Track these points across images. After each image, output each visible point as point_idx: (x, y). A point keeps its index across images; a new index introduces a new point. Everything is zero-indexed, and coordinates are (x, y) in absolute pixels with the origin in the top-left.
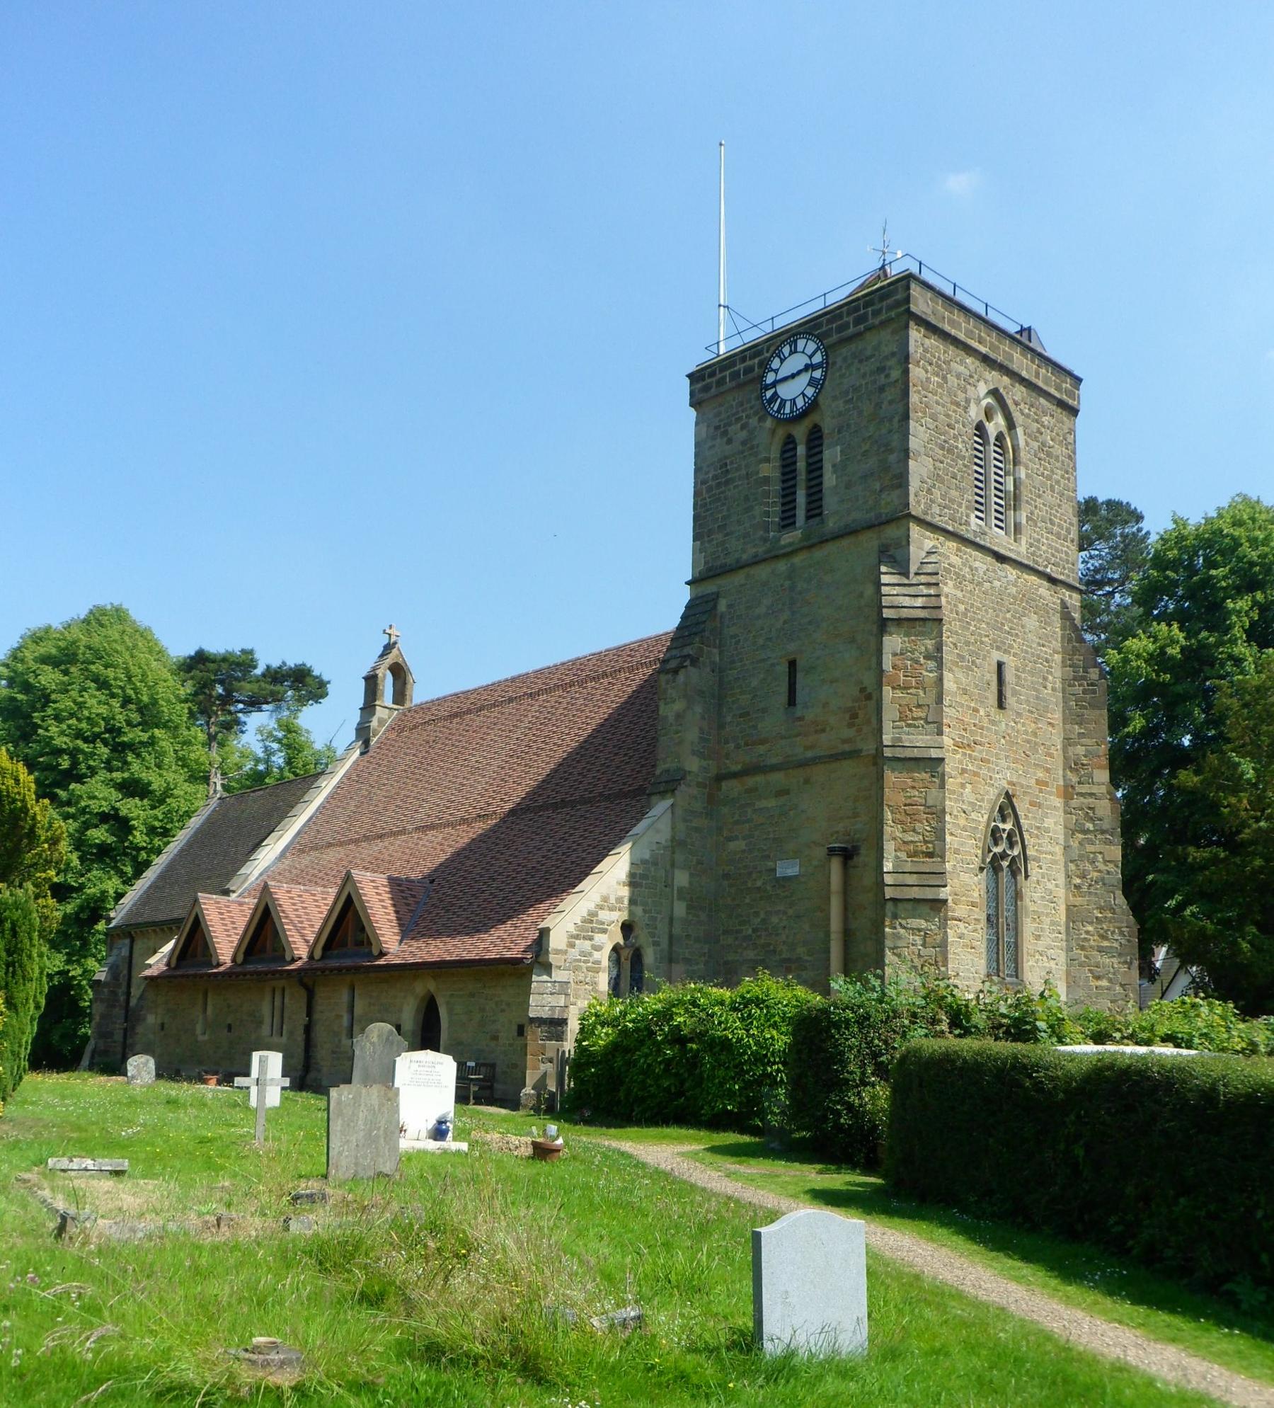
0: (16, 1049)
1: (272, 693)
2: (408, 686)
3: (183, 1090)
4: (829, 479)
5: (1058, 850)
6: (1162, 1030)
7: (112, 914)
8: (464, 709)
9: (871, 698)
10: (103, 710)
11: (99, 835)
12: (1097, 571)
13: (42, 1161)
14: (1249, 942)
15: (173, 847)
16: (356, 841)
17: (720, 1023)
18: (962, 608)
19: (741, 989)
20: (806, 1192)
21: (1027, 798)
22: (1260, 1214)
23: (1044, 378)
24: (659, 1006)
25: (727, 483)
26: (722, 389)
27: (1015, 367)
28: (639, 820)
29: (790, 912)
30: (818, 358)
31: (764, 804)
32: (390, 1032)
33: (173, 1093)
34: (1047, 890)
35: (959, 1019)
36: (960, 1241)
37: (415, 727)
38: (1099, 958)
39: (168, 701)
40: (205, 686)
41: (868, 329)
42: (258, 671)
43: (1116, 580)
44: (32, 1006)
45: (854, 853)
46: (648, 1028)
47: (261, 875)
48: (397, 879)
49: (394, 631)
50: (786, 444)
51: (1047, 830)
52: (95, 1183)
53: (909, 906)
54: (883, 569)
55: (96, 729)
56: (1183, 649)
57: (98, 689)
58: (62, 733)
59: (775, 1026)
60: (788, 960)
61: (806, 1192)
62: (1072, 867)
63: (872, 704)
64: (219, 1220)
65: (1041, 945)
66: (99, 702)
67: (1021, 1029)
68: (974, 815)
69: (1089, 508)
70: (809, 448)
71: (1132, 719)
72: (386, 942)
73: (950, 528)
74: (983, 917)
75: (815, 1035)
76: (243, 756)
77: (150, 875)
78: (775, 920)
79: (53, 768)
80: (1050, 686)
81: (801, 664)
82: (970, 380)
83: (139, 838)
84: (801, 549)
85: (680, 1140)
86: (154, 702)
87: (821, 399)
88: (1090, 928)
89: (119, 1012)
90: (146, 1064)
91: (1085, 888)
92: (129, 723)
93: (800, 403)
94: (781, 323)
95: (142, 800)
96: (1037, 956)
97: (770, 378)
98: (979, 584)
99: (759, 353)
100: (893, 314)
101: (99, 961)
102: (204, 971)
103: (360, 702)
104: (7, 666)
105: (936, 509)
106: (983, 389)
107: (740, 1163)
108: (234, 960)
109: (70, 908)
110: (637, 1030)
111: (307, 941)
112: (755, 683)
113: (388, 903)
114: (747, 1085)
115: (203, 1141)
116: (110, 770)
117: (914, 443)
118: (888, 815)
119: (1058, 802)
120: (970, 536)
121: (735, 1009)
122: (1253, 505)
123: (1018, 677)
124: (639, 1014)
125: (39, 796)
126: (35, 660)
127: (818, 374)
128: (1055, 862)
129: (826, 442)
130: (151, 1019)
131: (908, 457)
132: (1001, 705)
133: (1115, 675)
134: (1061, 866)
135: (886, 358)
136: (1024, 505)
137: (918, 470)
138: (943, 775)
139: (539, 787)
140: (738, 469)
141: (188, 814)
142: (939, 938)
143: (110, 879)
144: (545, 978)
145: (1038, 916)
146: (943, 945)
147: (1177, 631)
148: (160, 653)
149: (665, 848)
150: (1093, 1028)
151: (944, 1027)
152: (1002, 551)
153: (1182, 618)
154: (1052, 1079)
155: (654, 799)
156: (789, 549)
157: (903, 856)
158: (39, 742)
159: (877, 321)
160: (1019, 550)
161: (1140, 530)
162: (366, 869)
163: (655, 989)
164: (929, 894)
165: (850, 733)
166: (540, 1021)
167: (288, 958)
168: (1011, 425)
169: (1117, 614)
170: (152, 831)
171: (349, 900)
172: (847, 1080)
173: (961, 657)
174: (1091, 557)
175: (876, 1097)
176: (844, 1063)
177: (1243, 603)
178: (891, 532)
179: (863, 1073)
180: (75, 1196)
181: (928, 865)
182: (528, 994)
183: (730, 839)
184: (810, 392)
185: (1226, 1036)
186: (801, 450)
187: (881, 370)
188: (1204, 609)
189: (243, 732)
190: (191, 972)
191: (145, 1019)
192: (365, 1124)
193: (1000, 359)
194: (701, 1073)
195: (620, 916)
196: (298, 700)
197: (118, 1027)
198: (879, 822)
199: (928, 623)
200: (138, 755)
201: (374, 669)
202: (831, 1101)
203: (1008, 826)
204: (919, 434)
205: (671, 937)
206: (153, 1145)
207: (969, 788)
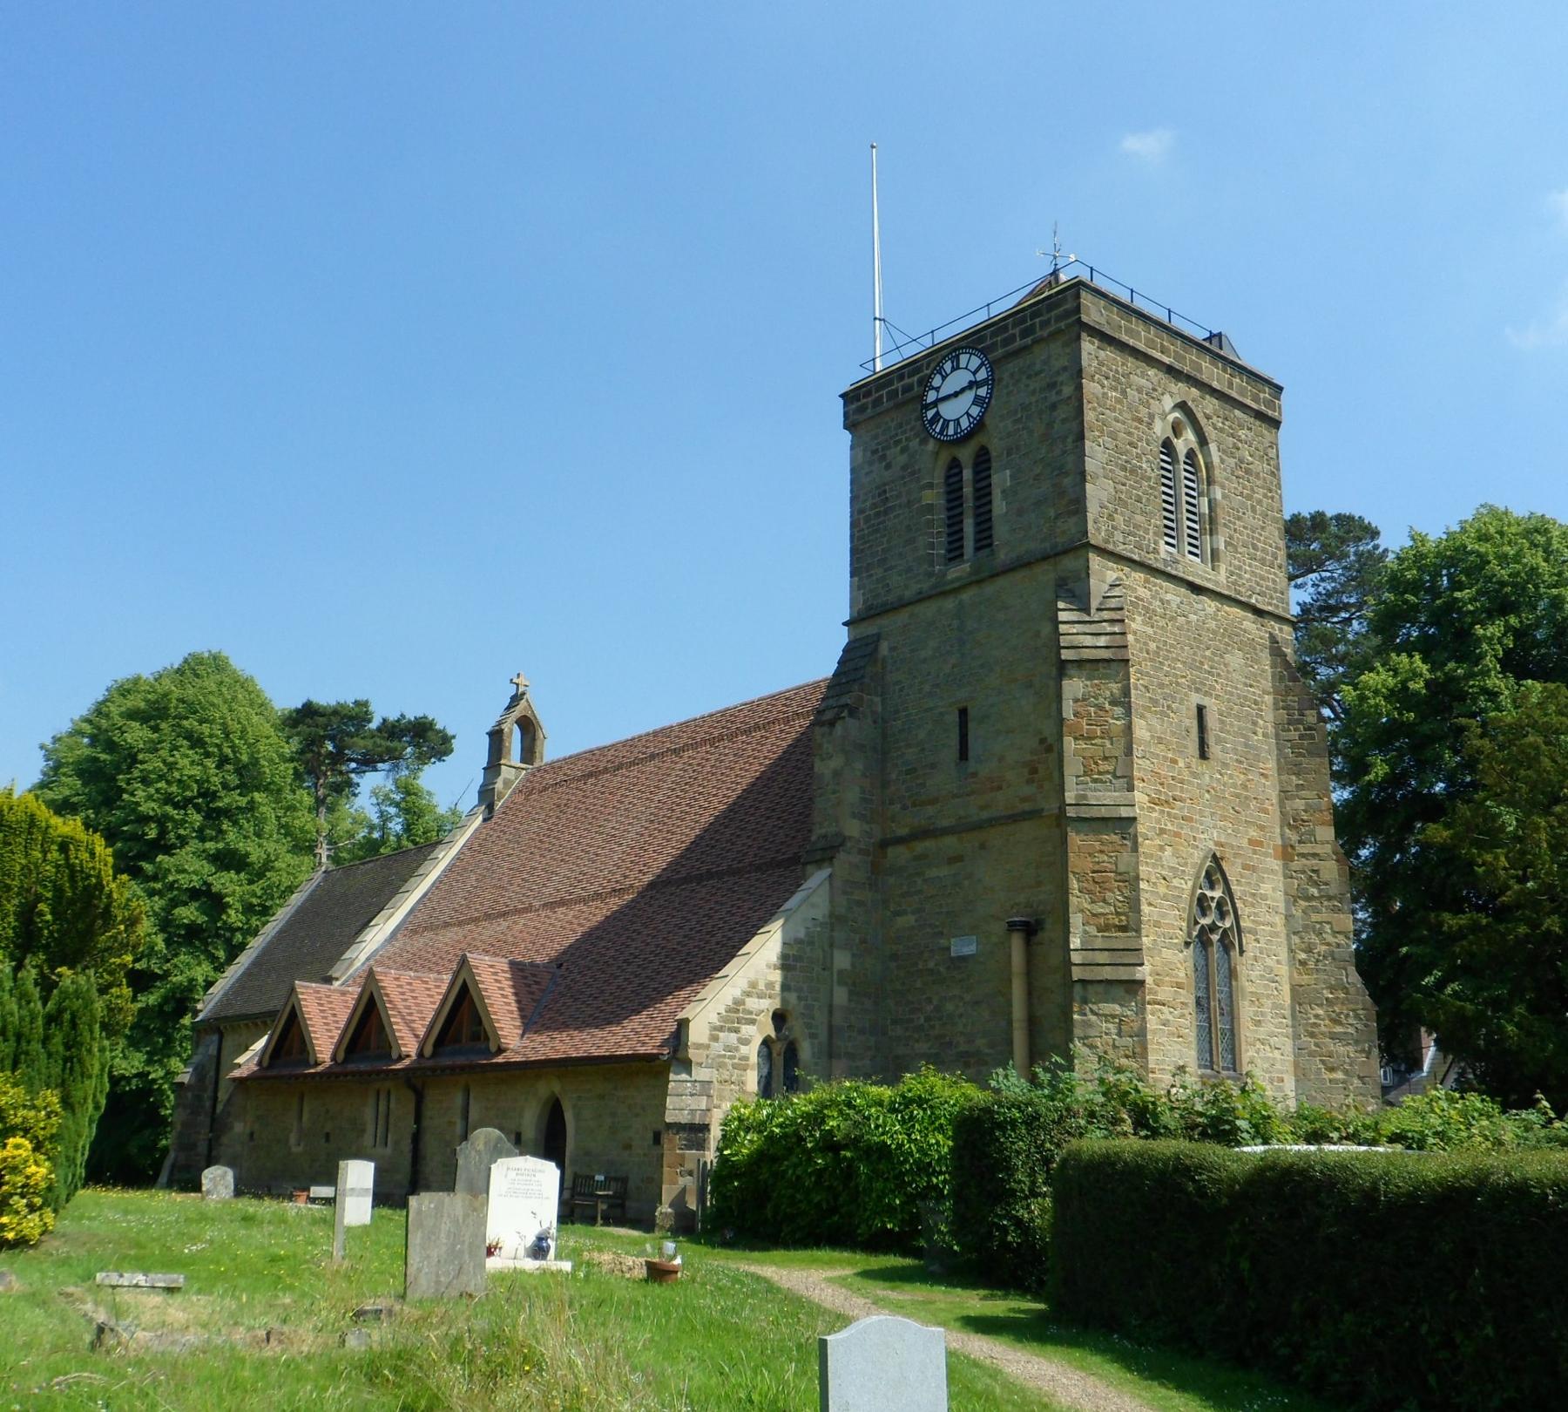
0: (71, 1153)
1: (389, 750)
2: (538, 743)
3: (267, 1207)
4: (999, 506)
5: (1279, 920)
6: (1389, 1128)
7: (199, 1006)
8: (598, 767)
9: (1051, 749)
10: (196, 771)
11: (188, 913)
12: (1329, 595)
13: (90, 1276)
14: (1517, 1025)
15: (271, 929)
16: (476, 920)
17: (877, 1127)
18: (1153, 646)
19: (902, 1088)
20: (957, 1320)
21: (1239, 861)
22: (1424, 1329)
23: (1237, 387)
24: (810, 1108)
25: (886, 512)
26: (879, 410)
27: (1204, 378)
28: (793, 893)
29: (967, 997)
30: (982, 375)
31: (933, 873)
32: (499, 1139)
33: (251, 1210)
34: (1267, 967)
35: (1144, 1118)
36: (1113, 1370)
37: (545, 789)
38: (1332, 1046)
39: (271, 761)
40: (313, 743)
41: (1035, 342)
42: (373, 725)
43: (1352, 605)
44: (91, 1106)
45: (1038, 927)
46: (796, 1133)
47: (368, 959)
48: (520, 963)
49: (521, 681)
50: (950, 468)
51: (1264, 897)
52: (144, 1298)
53: (1100, 988)
54: (1061, 605)
55: (188, 794)
56: (1428, 684)
57: (191, 748)
58: (150, 798)
59: (941, 1129)
60: (966, 1054)
61: (957, 1320)
62: (1296, 939)
63: (1054, 755)
64: (268, 1334)
65: (1262, 1032)
66: (192, 763)
67: (1220, 1129)
68: (1176, 882)
69: (1297, 530)
70: (976, 473)
71: (1372, 765)
72: (505, 1037)
73: (1136, 557)
74: (1191, 1000)
75: (977, 1133)
76: (355, 821)
77: (244, 960)
78: (950, 1007)
79: (136, 838)
80: (1260, 731)
81: (972, 713)
82: (1154, 393)
83: (234, 917)
84: (971, 584)
85: (830, 1264)
86: (255, 762)
87: (988, 421)
88: (1321, 1012)
89: (204, 1119)
90: (223, 1176)
91: (1311, 965)
92: (225, 786)
93: (965, 423)
94: (942, 336)
95: (238, 873)
96: (1258, 1045)
97: (931, 396)
98: (1172, 619)
99: (919, 370)
100: (1062, 325)
101: (182, 1060)
102: (298, 1071)
103: (483, 760)
104: (89, 721)
105: (1119, 537)
106: (1168, 402)
107: (893, 1289)
108: (334, 1058)
109: (152, 999)
110: (785, 1136)
111: (416, 1036)
112: (922, 735)
113: (509, 991)
114: (910, 1199)
115: (274, 1259)
116: (203, 839)
117: (1090, 465)
118: (1074, 884)
119: (1276, 864)
120: (1160, 566)
121: (893, 1110)
122: (1499, 516)
123: (1222, 722)
124: (787, 1118)
125: (118, 870)
126: (121, 715)
127: (983, 392)
128: (1276, 935)
129: (994, 465)
130: (239, 1127)
131: (1084, 480)
132: (1203, 755)
133: (1350, 716)
134: (1283, 939)
135: (1058, 373)
136: (1220, 529)
137: (1097, 493)
138: (1136, 836)
139: (681, 856)
140: (898, 496)
141: (291, 890)
142: (1136, 1026)
143: (199, 964)
144: (684, 1076)
145: (1257, 999)
146: (1141, 1033)
147: (1419, 663)
148: (263, 706)
149: (822, 924)
150: (1307, 1127)
151: (1127, 1127)
152: (1198, 581)
153: (1426, 648)
154: (1214, 1181)
155: (809, 868)
156: (956, 585)
157: (1093, 930)
158: (123, 808)
159: (1045, 333)
160: (1219, 579)
161: (1376, 547)
162: (486, 952)
163: (807, 1088)
164: (1122, 974)
165: (1028, 790)
166: (679, 1127)
167: (395, 1056)
168: (1203, 441)
169: (1356, 644)
170: (248, 909)
171: (464, 990)
172: (1014, 1191)
173: (1155, 702)
174: (1322, 580)
175: (1038, 1211)
176: (1010, 1170)
177: (1495, 629)
178: (1069, 563)
179: (1033, 1183)
180: (117, 1311)
181: (1120, 940)
182: (665, 1094)
183: (897, 914)
184: (975, 411)
185: (1464, 1134)
186: (967, 474)
187: (1052, 385)
188: (1450, 638)
189: (355, 795)
190: (285, 1072)
191: (232, 1128)
192: (448, 1237)
193: (1186, 369)
194: (857, 1186)
195: (770, 1004)
196: (418, 758)
197: (203, 1135)
198: (1064, 890)
199: (1115, 664)
200: (235, 823)
201: (500, 723)
202: (997, 1215)
203: (1217, 894)
204: (1096, 456)
205: (830, 1027)
206: (218, 1263)
207: (1169, 851)
